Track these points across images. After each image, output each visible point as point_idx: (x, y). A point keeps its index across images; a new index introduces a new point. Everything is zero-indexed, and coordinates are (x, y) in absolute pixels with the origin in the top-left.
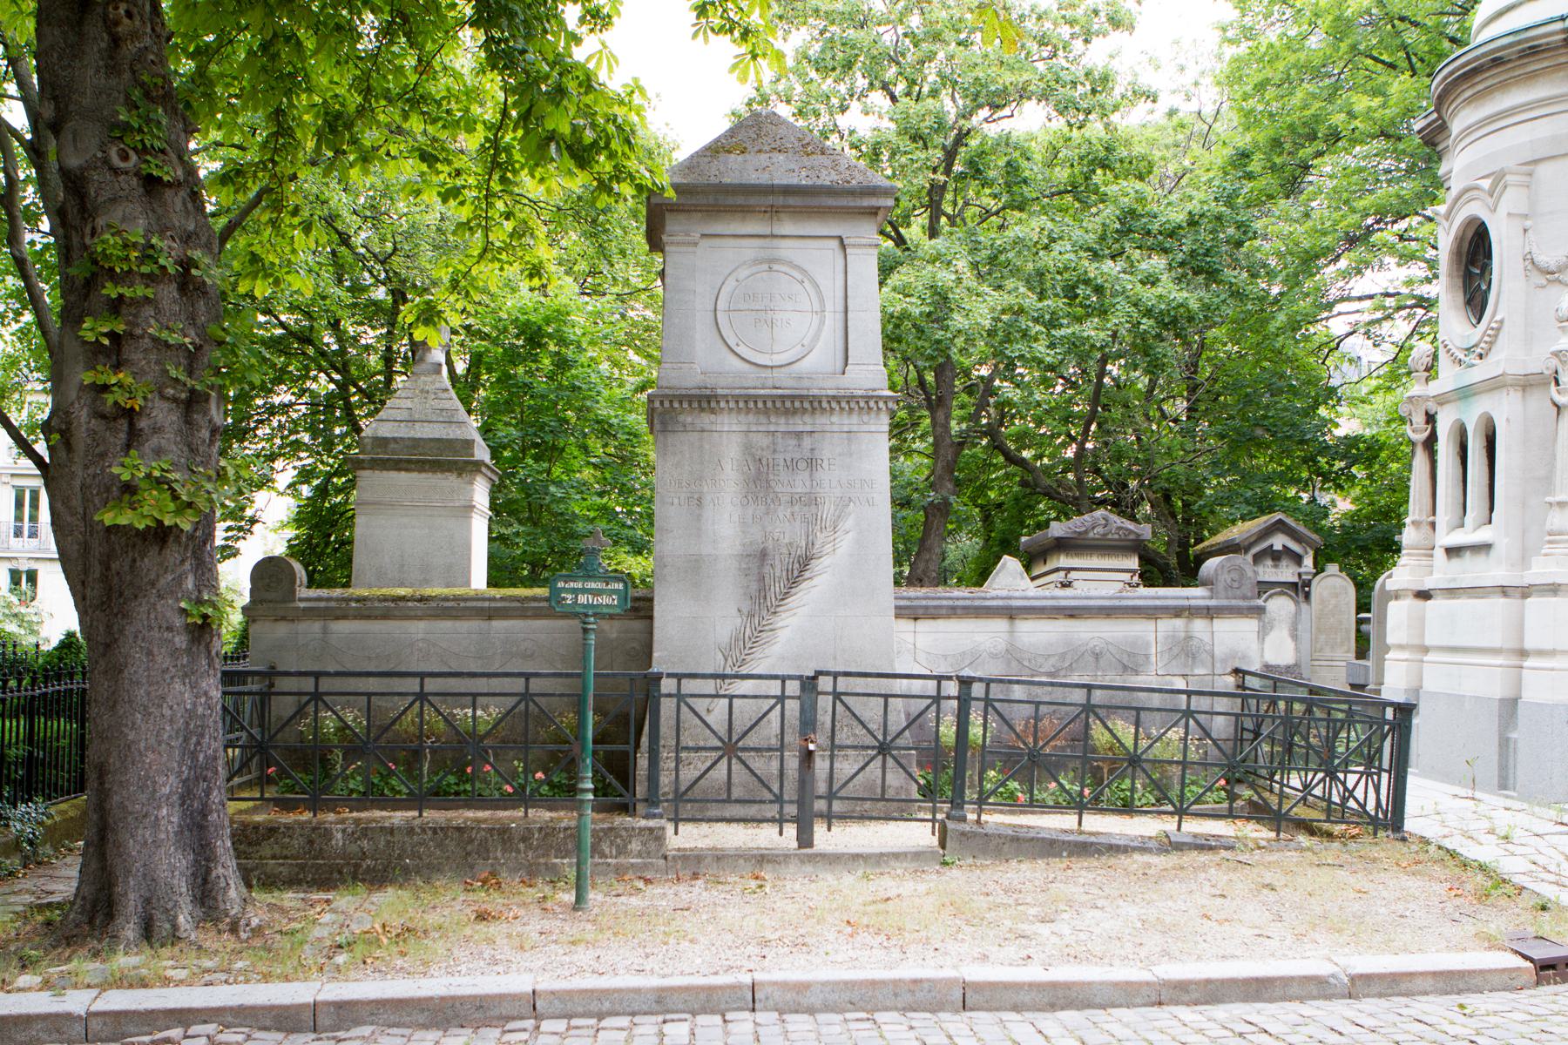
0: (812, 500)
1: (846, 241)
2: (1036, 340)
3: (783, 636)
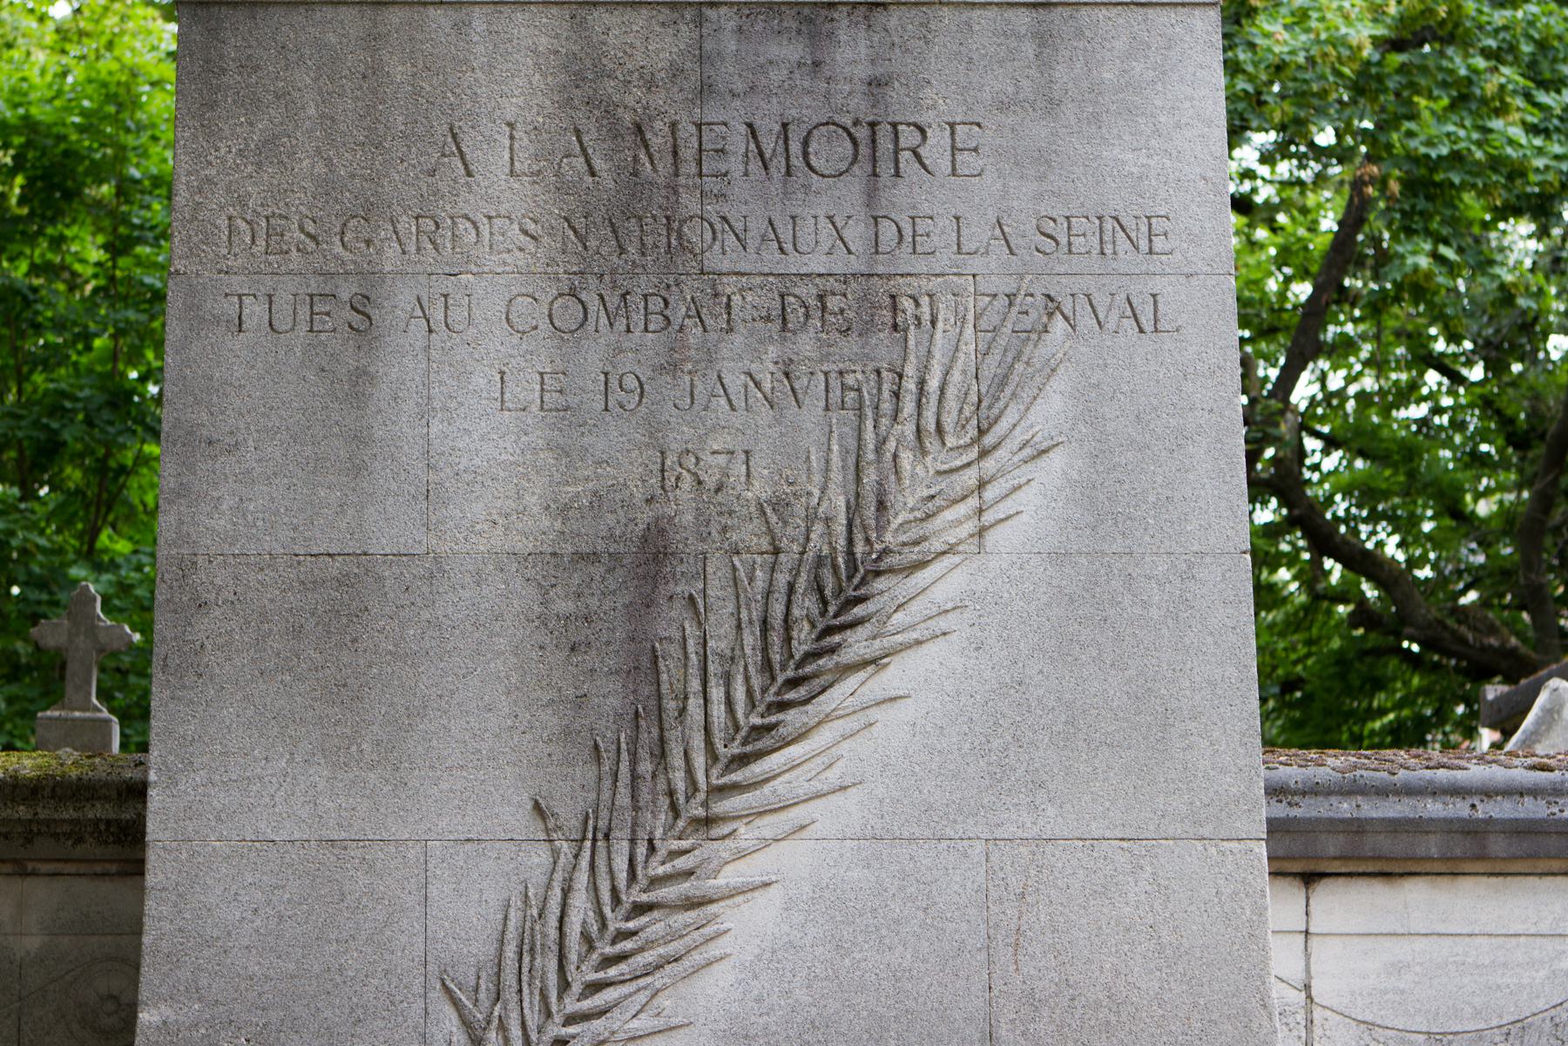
0: (875, 307)
2: (1502, 111)
3: (747, 927)
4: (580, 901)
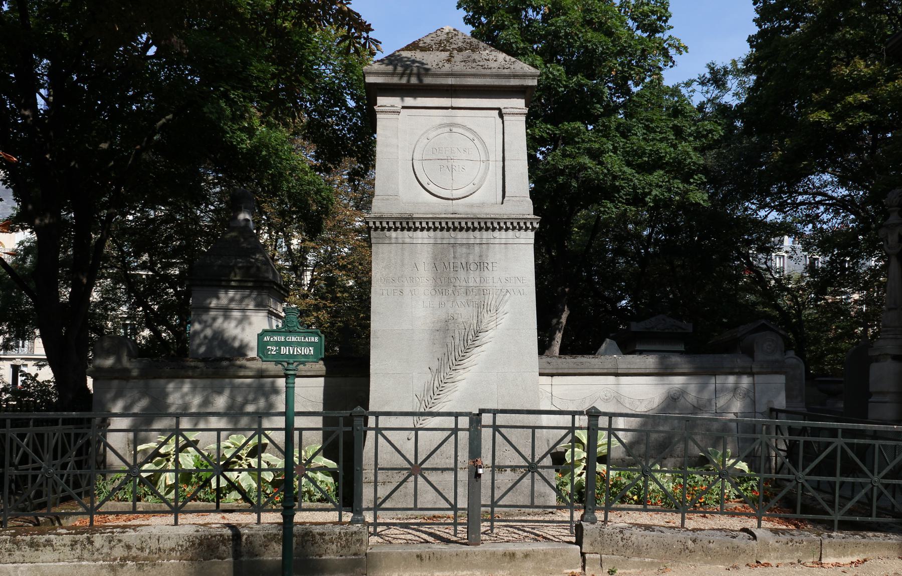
0: (482, 292)
1: (504, 111)
3: (461, 386)
4: (436, 382)
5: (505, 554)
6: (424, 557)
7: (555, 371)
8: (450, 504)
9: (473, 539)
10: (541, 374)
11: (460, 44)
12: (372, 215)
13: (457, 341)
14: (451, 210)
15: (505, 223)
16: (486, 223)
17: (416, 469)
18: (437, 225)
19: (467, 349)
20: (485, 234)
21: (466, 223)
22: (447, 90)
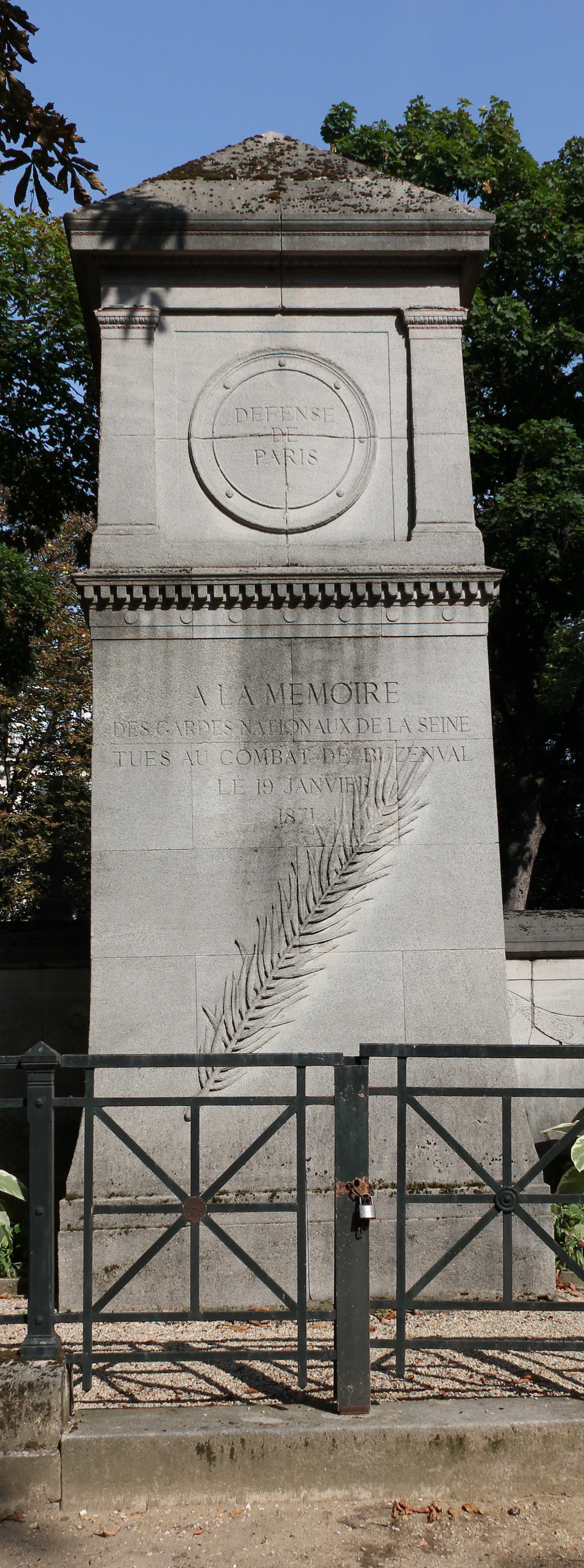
0: (363, 754)
1: (409, 316)
4: (254, 977)
5: (436, 1442)
6: (216, 1451)
7: (539, 948)
8: (287, 1300)
9: (346, 1397)
10: (510, 956)
11: (301, 166)
12: (92, 572)
13: (303, 875)
14: (283, 556)
15: (417, 586)
16: (369, 587)
17: (198, 1204)
18: (251, 592)
19: (329, 895)
20: (368, 614)
21: (322, 587)
22: (271, 268)
